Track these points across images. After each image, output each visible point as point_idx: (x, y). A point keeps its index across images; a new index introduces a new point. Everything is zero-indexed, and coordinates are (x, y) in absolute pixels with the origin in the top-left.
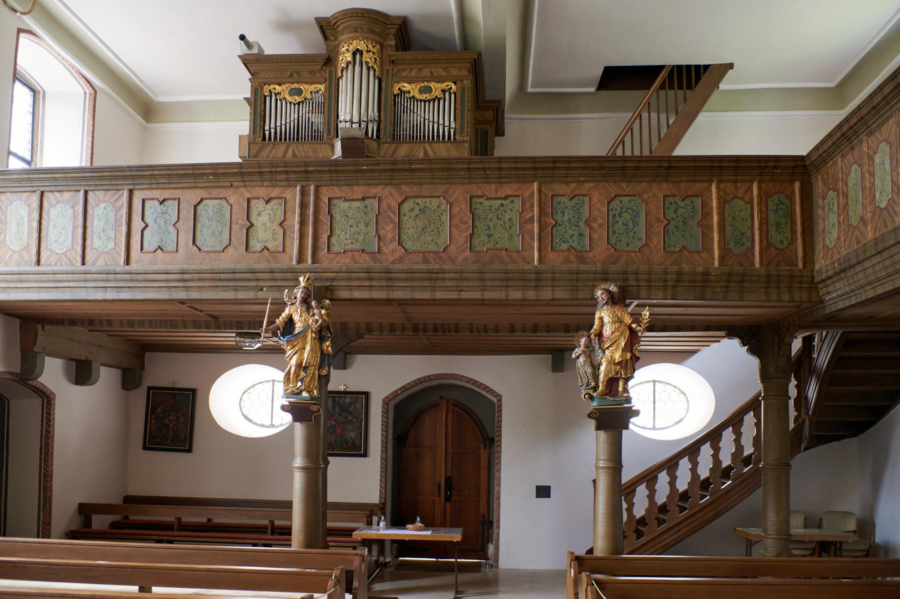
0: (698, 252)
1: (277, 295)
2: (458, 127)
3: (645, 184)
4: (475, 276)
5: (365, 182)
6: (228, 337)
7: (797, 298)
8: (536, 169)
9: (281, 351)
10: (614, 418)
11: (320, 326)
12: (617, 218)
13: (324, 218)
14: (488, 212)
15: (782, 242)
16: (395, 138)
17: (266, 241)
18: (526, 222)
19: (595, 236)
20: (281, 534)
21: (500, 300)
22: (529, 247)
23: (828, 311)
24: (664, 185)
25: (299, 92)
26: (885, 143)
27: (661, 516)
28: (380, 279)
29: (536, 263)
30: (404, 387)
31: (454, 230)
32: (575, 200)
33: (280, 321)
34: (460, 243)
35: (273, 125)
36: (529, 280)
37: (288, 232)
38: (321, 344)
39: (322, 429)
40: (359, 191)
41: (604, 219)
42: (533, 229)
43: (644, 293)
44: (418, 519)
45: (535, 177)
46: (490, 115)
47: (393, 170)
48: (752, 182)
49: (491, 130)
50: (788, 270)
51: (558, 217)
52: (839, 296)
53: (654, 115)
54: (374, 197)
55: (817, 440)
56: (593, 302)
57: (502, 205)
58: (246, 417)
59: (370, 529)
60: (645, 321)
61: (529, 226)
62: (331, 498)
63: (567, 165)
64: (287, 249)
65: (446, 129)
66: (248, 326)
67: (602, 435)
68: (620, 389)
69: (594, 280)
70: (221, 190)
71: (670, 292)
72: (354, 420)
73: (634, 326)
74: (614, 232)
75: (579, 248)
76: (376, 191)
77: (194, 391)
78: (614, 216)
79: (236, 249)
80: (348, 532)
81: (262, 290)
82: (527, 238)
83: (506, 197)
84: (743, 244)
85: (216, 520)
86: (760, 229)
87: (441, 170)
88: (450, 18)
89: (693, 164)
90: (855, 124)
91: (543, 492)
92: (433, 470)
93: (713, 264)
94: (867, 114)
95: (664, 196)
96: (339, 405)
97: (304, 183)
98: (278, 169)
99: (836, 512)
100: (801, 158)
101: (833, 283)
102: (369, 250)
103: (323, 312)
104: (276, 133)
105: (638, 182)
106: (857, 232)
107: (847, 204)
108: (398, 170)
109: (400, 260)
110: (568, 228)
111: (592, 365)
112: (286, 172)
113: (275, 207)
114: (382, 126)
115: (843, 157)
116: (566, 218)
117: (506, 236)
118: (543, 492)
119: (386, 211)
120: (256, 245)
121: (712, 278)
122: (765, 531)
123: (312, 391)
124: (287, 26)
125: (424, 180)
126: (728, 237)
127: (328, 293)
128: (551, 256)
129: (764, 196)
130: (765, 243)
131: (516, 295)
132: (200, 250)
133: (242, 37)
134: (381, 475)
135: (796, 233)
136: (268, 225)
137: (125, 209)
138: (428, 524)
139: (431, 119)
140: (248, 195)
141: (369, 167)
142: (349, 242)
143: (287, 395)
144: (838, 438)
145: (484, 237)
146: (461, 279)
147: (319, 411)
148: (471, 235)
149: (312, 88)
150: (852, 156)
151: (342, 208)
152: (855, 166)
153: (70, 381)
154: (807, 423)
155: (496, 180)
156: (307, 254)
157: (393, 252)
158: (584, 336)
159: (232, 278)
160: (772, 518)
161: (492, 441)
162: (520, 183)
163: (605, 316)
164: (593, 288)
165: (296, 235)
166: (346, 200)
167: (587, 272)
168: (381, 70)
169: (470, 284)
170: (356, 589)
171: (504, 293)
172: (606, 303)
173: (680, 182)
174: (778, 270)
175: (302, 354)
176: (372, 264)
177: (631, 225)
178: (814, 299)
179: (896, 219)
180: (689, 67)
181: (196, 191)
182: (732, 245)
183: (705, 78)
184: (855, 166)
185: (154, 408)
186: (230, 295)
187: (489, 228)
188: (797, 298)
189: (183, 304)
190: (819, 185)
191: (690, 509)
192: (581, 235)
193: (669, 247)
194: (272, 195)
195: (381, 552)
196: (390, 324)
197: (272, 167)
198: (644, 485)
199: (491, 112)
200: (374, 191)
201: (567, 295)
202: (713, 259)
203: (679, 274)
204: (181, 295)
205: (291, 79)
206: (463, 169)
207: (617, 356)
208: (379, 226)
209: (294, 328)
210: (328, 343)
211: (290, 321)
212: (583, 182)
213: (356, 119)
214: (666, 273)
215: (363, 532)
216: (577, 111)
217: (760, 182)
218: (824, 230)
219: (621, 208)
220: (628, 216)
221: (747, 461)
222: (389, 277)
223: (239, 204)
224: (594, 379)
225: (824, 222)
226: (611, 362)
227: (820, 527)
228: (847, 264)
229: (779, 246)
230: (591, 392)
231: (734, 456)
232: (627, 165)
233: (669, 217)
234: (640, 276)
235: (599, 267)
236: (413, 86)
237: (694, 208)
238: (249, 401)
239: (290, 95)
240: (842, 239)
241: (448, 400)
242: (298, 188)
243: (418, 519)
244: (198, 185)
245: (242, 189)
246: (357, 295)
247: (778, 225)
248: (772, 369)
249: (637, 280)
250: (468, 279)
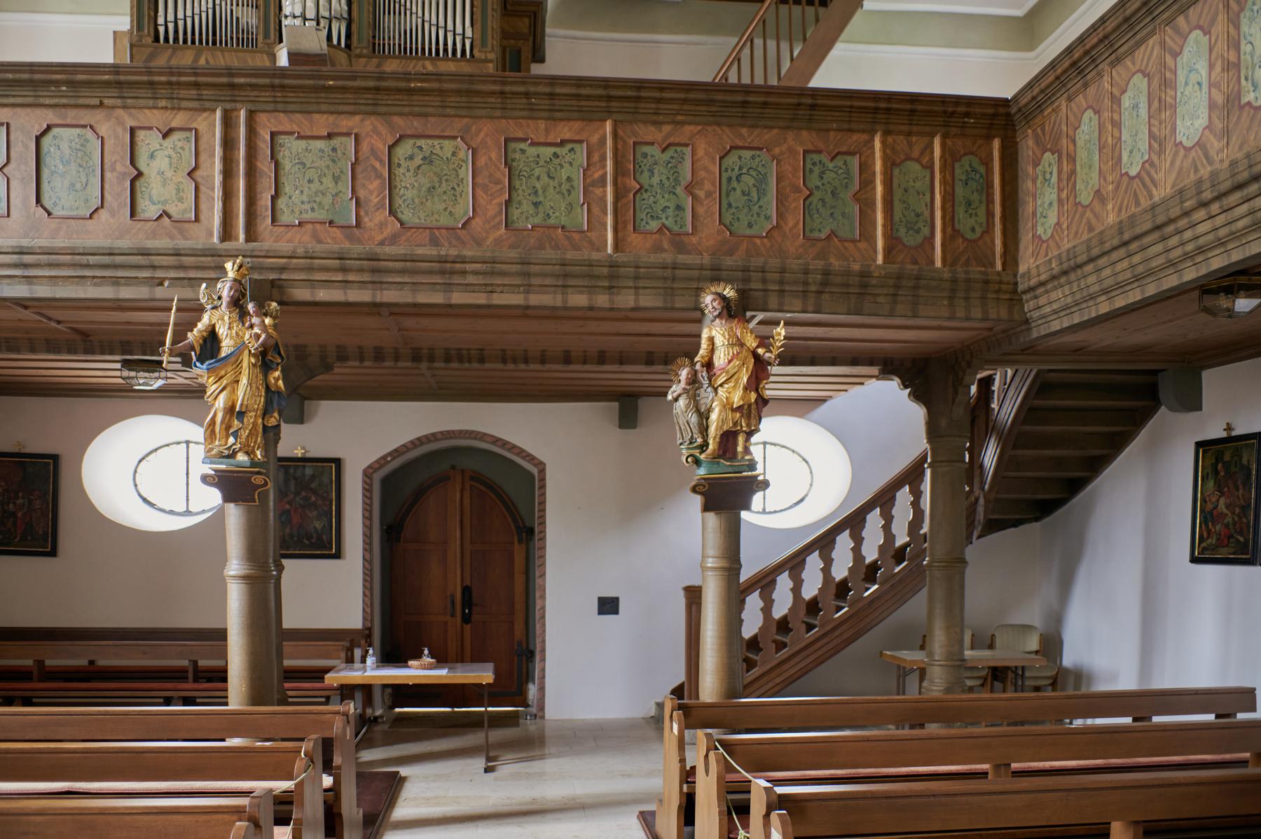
0: (854, 241)
1: (188, 293)
2: (478, 36)
3: (776, 131)
4: (515, 268)
5: (332, 108)
6: (107, 370)
7: (993, 315)
8: (610, 98)
9: (198, 392)
10: (728, 493)
11: (263, 345)
12: (734, 184)
14: (533, 165)
15: (973, 230)
17: (165, 202)
18: (594, 184)
19: (701, 210)
20: (209, 680)
21: (554, 308)
22: (595, 223)
23: (1035, 335)
24: (805, 133)
26: (1139, 75)
27: (779, 638)
28: (360, 270)
29: (610, 250)
30: (396, 450)
31: (480, 192)
32: (670, 152)
33: (194, 336)
34: (490, 214)
35: (171, 17)
36: (598, 277)
37: (203, 188)
38: (266, 376)
39: (271, 514)
40: (322, 123)
41: (714, 185)
42: (605, 196)
43: (773, 301)
44: (426, 652)
45: (609, 112)
46: (523, 25)
47: (377, 89)
48: (933, 136)
49: (526, 53)
50: (981, 272)
51: (644, 178)
52: (1055, 312)
53: (771, 44)
54: (348, 134)
55: (993, 526)
56: (697, 314)
57: (556, 155)
58: (145, 500)
59: (352, 670)
60: (778, 344)
61: (598, 191)
62: (286, 624)
63: (657, 95)
64: (202, 217)
65: (458, 39)
66: (139, 348)
67: (712, 517)
68: (740, 449)
69: (699, 280)
70: (82, 112)
71: (811, 301)
72: (320, 502)
73: (760, 351)
74: (730, 205)
75: (676, 228)
76: (350, 124)
77: (55, 458)
78: (730, 179)
79: (113, 215)
81: (161, 284)
82: (596, 210)
83: (563, 143)
84: (918, 231)
85: (102, 662)
86: (943, 208)
87: (459, 92)
89: (848, 103)
90: (1093, 47)
91: (608, 606)
92: (444, 577)
93: (875, 260)
94: (1114, 30)
95: (805, 152)
96: (296, 479)
97: (228, 106)
98: (183, 79)
99: (1012, 626)
100: (1004, 102)
101: (1047, 292)
102: (342, 223)
103: (268, 321)
104: (176, 31)
105: (766, 127)
106: (1089, 214)
107: (1073, 173)
108: (387, 89)
109: (393, 239)
110: (659, 196)
111: (698, 411)
112: (197, 85)
113: (179, 144)
114: (354, 28)
115: (1070, 99)
116: (655, 180)
117: (563, 206)
118: (608, 606)
119: (368, 158)
120: (149, 209)
121: (874, 282)
122: (930, 655)
123: (253, 452)
125: (430, 110)
126: (896, 218)
127: (275, 292)
128: (634, 239)
129: (950, 159)
130: (949, 230)
131: (579, 300)
132: (49, 214)
134: (364, 586)
135: (993, 216)
136: (169, 174)
138: (441, 659)
139: (434, 21)
140: (130, 122)
141: (340, 83)
142: (307, 206)
143: (208, 459)
144: (1016, 523)
145: (527, 207)
146: (492, 273)
147: (266, 484)
148: (508, 203)
150: (1085, 97)
151: (294, 151)
152: (1089, 113)
154: (982, 501)
155: (545, 114)
156: (237, 226)
157: (382, 225)
158: (684, 366)
159: (109, 262)
160: (939, 640)
161: (531, 531)
162: (583, 120)
163: (717, 336)
164: (698, 291)
165: (218, 193)
166: (300, 137)
169: (507, 281)
170: (339, 768)
171: (559, 297)
172: (719, 316)
173: (828, 130)
174: (967, 272)
175: (234, 391)
176: (347, 245)
177: (754, 194)
178: (1017, 317)
179: (1155, 192)
181: (38, 111)
182: (902, 232)
184: (1089, 113)
186: (106, 292)
187: (536, 193)
188: (993, 315)
189: (26, 307)
190: (1027, 145)
191: (822, 626)
193: (811, 231)
194: (174, 125)
195: (368, 702)
196: (375, 348)
197: (172, 74)
198: (757, 592)
199: (526, 21)
200: (346, 123)
201: (659, 303)
202: (875, 252)
203: (826, 273)
204: (20, 291)
206: (493, 93)
207: (737, 399)
208: (358, 183)
209: (219, 348)
210: (277, 374)
211: (212, 338)
212: (683, 123)
213: (311, 14)
214: (806, 272)
215: (342, 674)
216: (653, 29)
217: (945, 137)
218: (1034, 214)
219: (740, 168)
221: (900, 555)
222: (375, 266)
223: (116, 137)
224: (701, 433)
225: (1035, 199)
226: (728, 406)
227: (991, 646)
228: (1072, 263)
229: (970, 236)
230: (696, 453)
231: (882, 549)
232: (750, 99)
233: (811, 185)
234: (769, 276)
235: (706, 260)
237: (848, 172)
240: (1065, 226)
241: (463, 471)
242: (218, 113)
243: (426, 652)
244: (42, 100)
245: (120, 112)
246: (323, 295)
247: (969, 204)
248: (943, 423)
249: (764, 281)
250: (503, 274)
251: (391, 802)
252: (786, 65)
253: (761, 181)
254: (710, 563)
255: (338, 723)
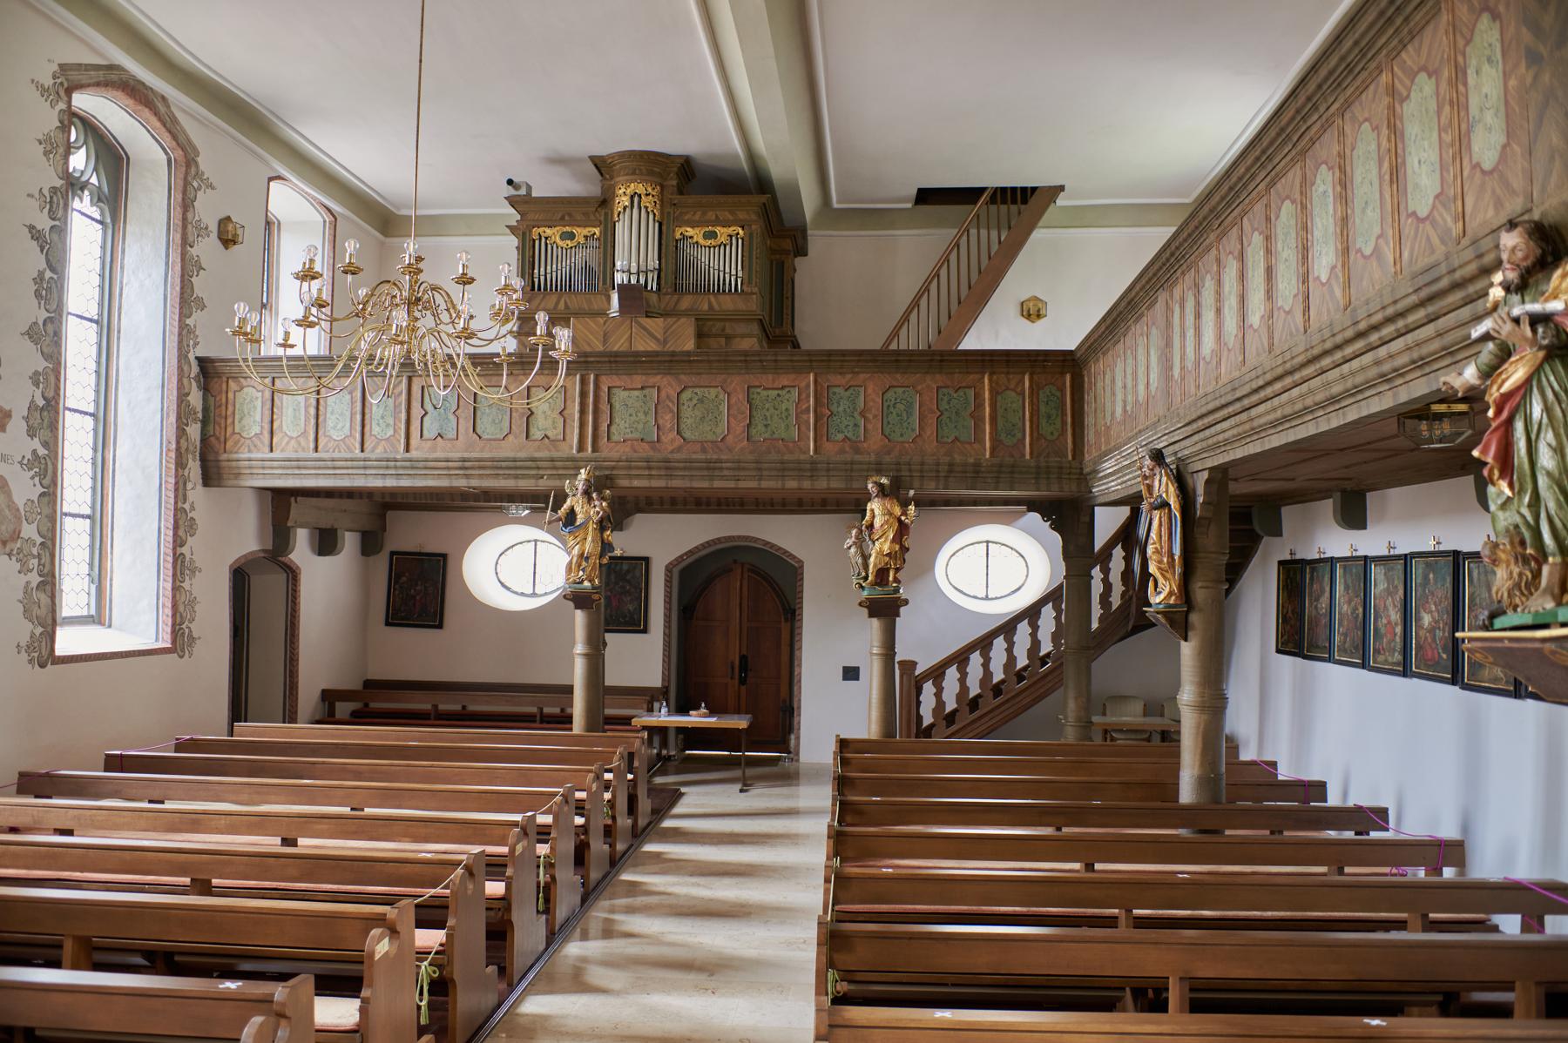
13: (604, 407)
16: (676, 289)
19: (870, 427)
22: (803, 437)
25: (571, 236)
28: (659, 468)
33: (562, 512)
40: (638, 380)
45: (811, 369)
53: (984, 232)
67: (875, 622)
77: (444, 556)
80: (626, 721)
82: (803, 428)
85: (472, 708)
88: (737, 156)
92: (726, 648)
109: (679, 449)
120: (537, 434)
124: (559, 161)
128: (827, 446)
133: (510, 182)
137: (404, 396)
138: (713, 711)
145: (760, 427)
146: (739, 469)
148: (749, 426)
149: (586, 231)
153: (313, 550)
157: (672, 441)
164: (867, 478)
165: (576, 424)
167: (861, 463)
168: (662, 213)
180: (1014, 189)
182: (1003, 436)
183: (1033, 201)
185: (398, 577)
192: (856, 425)
195: (664, 744)
200: (656, 380)
205: (562, 221)
207: (886, 548)
211: (572, 514)
213: (634, 270)
214: (938, 464)
220: (902, 407)
222: (668, 466)
227: (1162, 715)
235: (873, 458)
236: (697, 230)
238: (515, 569)
239: (562, 238)
241: (743, 565)
247: (1049, 417)
251: (673, 804)
252: (995, 247)
253: (910, 406)
254: (875, 651)
255: (637, 743)
